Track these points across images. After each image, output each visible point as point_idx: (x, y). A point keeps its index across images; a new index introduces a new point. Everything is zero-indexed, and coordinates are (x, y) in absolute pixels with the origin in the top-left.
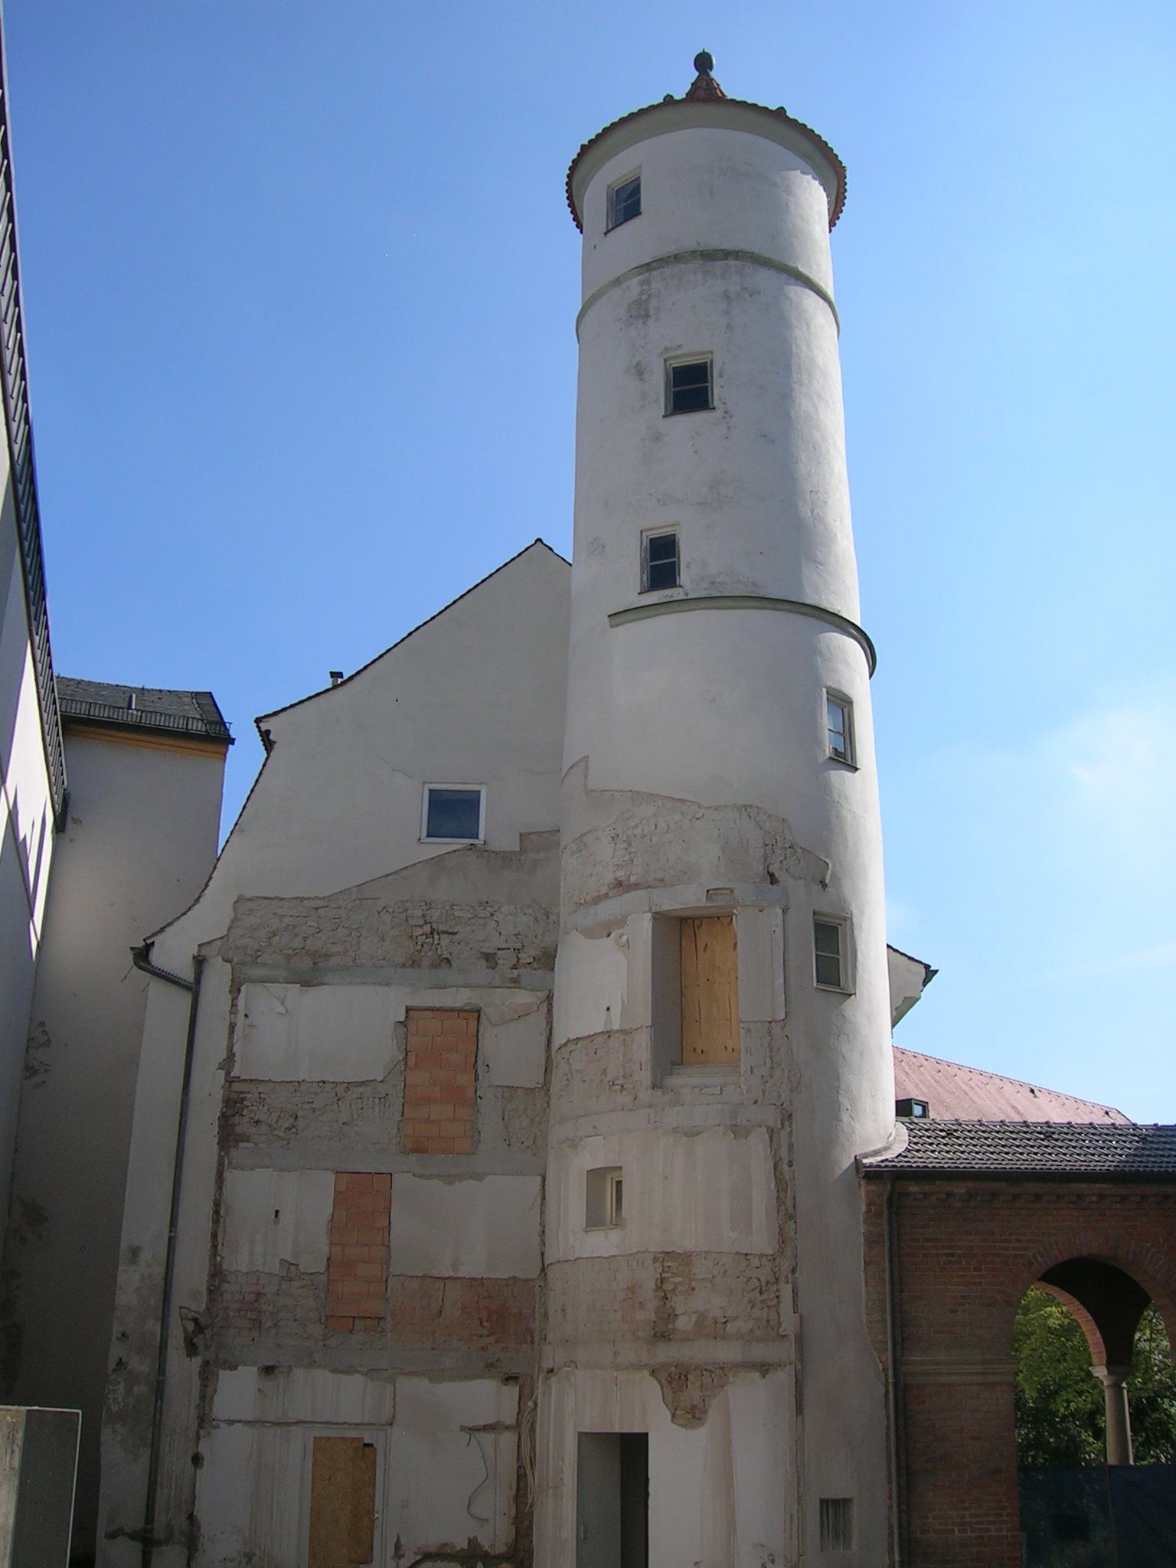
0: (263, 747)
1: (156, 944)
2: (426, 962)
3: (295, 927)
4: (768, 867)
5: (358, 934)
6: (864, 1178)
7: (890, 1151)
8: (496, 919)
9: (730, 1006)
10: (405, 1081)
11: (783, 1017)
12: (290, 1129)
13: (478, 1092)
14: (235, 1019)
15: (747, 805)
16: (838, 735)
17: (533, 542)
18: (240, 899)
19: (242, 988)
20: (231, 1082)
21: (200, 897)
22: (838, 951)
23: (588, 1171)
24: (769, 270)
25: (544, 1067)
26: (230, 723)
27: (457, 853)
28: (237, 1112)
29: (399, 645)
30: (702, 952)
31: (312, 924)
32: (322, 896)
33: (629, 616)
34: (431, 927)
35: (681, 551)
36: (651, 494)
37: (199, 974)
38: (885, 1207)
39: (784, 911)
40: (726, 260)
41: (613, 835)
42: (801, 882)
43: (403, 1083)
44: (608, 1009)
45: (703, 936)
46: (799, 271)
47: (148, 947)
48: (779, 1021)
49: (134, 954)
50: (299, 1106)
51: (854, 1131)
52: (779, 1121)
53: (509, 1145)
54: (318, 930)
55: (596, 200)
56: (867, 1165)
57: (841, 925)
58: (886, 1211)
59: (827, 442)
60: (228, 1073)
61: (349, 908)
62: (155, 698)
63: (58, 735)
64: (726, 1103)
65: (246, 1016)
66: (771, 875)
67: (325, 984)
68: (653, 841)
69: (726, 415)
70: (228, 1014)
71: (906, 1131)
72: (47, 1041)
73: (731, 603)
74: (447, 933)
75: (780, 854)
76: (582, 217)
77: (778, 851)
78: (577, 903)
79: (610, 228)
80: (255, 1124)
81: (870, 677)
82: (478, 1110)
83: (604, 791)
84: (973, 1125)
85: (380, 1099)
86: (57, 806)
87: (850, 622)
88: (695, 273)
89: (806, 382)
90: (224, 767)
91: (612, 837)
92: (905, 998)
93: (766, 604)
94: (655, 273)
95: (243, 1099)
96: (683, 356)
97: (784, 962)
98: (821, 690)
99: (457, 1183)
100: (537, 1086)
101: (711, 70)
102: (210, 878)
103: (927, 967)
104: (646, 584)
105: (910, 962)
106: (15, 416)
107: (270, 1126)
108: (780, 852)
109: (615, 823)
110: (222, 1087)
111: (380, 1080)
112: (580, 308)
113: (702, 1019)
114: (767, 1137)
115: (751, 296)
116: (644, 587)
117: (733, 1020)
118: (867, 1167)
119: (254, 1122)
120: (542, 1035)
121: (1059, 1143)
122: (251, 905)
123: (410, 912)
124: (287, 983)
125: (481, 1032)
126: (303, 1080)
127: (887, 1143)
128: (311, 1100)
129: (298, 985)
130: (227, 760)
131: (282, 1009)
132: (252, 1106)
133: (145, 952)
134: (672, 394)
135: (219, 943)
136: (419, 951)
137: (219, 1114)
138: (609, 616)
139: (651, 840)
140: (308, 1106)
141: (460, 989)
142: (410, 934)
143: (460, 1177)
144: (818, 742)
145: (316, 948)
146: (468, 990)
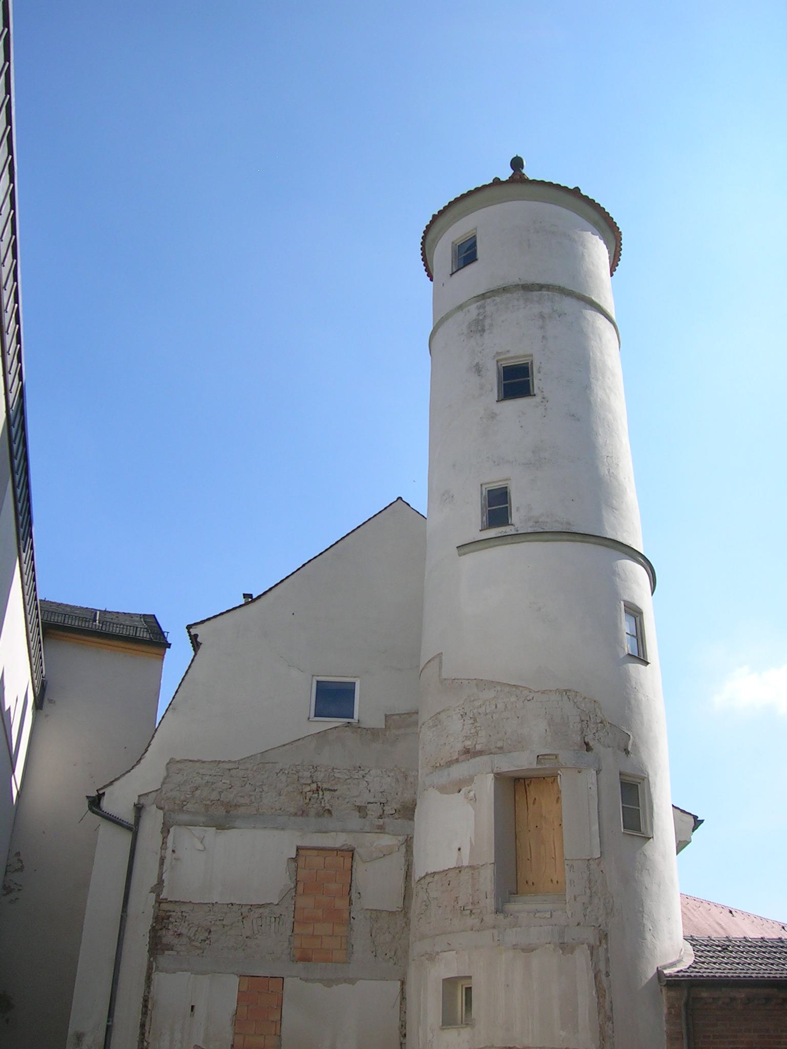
0: (192, 648)
1: (106, 793)
2: (313, 812)
3: (213, 783)
4: (584, 738)
5: (261, 790)
6: (665, 986)
7: (682, 963)
8: (366, 780)
9: (554, 848)
10: (295, 905)
11: (599, 856)
12: (205, 941)
13: (351, 914)
14: (165, 853)
15: (567, 690)
16: (633, 638)
17: (395, 500)
18: (172, 762)
19: (170, 830)
20: (160, 903)
21: (141, 759)
22: (639, 804)
23: (443, 980)
24: (571, 298)
25: (403, 895)
26: (168, 633)
27: (337, 729)
28: (164, 927)
29: (295, 574)
30: (532, 805)
31: (226, 781)
32: (234, 760)
33: (472, 547)
34: (317, 785)
35: (512, 500)
36: (488, 457)
37: (138, 818)
38: (683, 1009)
39: (598, 772)
40: (541, 291)
41: (462, 713)
42: (610, 750)
43: (293, 906)
44: (459, 849)
45: (532, 791)
46: (593, 300)
47: (100, 796)
48: (596, 859)
49: (89, 801)
50: (213, 922)
51: (655, 948)
52: (597, 939)
53: (375, 956)
54: (230, 786)
55: (443, 253)
56: (668, 975)
57: (640, 783)
58: (683, 1013)
59: (617, 422)
60: (158, 895)
61: (254, 769)
62: (114, 617)
63: (39, 634)
64: (555, 925)
65: (173, 851)
66: (587, 744)
67: (234, 828)
68: (494, 718)
69: (543, 400)
70: (160, 850)
71: (691, 947)
72: (21, 866)
73: (550, 537)
74: (329, 790)
75: (593, 728)
76: (433, 269)
77: (592, 725)
78: (433, 766)
79: (454, 270)
80: (178, 936)
81: (652, 593)
82: (351, 928)
83: (454, 679)
84: (740, 942)
85: (275, 918)
86: (37, 688)
87: (637, 551)
88: (518, 300)
89: (601, 378)
90: (162, 665)
91: (461, 715)
92: (680, 841)
93: (578, 538)
94: (489, 300)
95: (169, 916)
96: (512, 358)
97: (598, 812)
98: (620, 602)
99: (335, 986)
100: (398, 909)
101: (522, 168)
102: (149, 745)
103: (695, 817)
104: (485, 524)
105: (682, 813)
106: (10, 369)
107: (189, 938)
108: (593, 726)
109: (463, 704)
110: (153, 906)
111: (277, 903)
112: (432, 329)
113: (533, 858)
114: (589, 952)
115: (559, 316)
116: (484, 525)
117: (557, 858)
118: (669, 977)
119: (177, 934)
120: (401, 869)
121: (734, 955)
122: (179, 766)
123: (301, 774)
124: (206, 826)
125: (354, 866)
126: (216, 903)
127: (680, 956)
128: (222, 918)
129: (215, 828)
130: (165, 660)
131: (201, 847)
132: (176, 922)
133: (97, 800)
134: (503, 386)
135: (154, 794)
136: (308, 804)
137: (150, 928)
138: (457, 547)
139: (492, 717)
140: (218, 923)
141: (339, 833)
142: (301, 791)
143: (337, 981)
144: (617, 641)
145: (228, 800)
146: (344, 834)
